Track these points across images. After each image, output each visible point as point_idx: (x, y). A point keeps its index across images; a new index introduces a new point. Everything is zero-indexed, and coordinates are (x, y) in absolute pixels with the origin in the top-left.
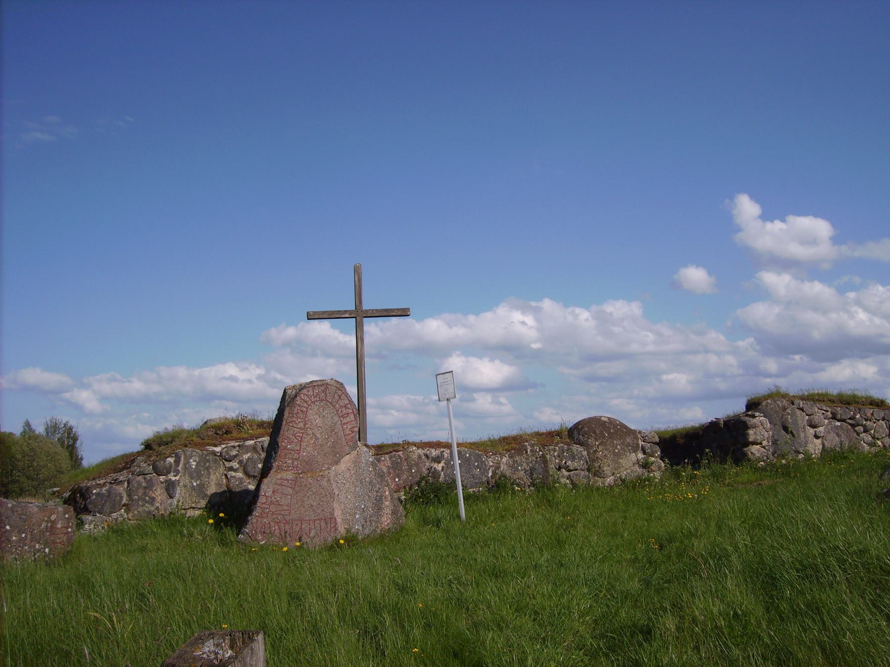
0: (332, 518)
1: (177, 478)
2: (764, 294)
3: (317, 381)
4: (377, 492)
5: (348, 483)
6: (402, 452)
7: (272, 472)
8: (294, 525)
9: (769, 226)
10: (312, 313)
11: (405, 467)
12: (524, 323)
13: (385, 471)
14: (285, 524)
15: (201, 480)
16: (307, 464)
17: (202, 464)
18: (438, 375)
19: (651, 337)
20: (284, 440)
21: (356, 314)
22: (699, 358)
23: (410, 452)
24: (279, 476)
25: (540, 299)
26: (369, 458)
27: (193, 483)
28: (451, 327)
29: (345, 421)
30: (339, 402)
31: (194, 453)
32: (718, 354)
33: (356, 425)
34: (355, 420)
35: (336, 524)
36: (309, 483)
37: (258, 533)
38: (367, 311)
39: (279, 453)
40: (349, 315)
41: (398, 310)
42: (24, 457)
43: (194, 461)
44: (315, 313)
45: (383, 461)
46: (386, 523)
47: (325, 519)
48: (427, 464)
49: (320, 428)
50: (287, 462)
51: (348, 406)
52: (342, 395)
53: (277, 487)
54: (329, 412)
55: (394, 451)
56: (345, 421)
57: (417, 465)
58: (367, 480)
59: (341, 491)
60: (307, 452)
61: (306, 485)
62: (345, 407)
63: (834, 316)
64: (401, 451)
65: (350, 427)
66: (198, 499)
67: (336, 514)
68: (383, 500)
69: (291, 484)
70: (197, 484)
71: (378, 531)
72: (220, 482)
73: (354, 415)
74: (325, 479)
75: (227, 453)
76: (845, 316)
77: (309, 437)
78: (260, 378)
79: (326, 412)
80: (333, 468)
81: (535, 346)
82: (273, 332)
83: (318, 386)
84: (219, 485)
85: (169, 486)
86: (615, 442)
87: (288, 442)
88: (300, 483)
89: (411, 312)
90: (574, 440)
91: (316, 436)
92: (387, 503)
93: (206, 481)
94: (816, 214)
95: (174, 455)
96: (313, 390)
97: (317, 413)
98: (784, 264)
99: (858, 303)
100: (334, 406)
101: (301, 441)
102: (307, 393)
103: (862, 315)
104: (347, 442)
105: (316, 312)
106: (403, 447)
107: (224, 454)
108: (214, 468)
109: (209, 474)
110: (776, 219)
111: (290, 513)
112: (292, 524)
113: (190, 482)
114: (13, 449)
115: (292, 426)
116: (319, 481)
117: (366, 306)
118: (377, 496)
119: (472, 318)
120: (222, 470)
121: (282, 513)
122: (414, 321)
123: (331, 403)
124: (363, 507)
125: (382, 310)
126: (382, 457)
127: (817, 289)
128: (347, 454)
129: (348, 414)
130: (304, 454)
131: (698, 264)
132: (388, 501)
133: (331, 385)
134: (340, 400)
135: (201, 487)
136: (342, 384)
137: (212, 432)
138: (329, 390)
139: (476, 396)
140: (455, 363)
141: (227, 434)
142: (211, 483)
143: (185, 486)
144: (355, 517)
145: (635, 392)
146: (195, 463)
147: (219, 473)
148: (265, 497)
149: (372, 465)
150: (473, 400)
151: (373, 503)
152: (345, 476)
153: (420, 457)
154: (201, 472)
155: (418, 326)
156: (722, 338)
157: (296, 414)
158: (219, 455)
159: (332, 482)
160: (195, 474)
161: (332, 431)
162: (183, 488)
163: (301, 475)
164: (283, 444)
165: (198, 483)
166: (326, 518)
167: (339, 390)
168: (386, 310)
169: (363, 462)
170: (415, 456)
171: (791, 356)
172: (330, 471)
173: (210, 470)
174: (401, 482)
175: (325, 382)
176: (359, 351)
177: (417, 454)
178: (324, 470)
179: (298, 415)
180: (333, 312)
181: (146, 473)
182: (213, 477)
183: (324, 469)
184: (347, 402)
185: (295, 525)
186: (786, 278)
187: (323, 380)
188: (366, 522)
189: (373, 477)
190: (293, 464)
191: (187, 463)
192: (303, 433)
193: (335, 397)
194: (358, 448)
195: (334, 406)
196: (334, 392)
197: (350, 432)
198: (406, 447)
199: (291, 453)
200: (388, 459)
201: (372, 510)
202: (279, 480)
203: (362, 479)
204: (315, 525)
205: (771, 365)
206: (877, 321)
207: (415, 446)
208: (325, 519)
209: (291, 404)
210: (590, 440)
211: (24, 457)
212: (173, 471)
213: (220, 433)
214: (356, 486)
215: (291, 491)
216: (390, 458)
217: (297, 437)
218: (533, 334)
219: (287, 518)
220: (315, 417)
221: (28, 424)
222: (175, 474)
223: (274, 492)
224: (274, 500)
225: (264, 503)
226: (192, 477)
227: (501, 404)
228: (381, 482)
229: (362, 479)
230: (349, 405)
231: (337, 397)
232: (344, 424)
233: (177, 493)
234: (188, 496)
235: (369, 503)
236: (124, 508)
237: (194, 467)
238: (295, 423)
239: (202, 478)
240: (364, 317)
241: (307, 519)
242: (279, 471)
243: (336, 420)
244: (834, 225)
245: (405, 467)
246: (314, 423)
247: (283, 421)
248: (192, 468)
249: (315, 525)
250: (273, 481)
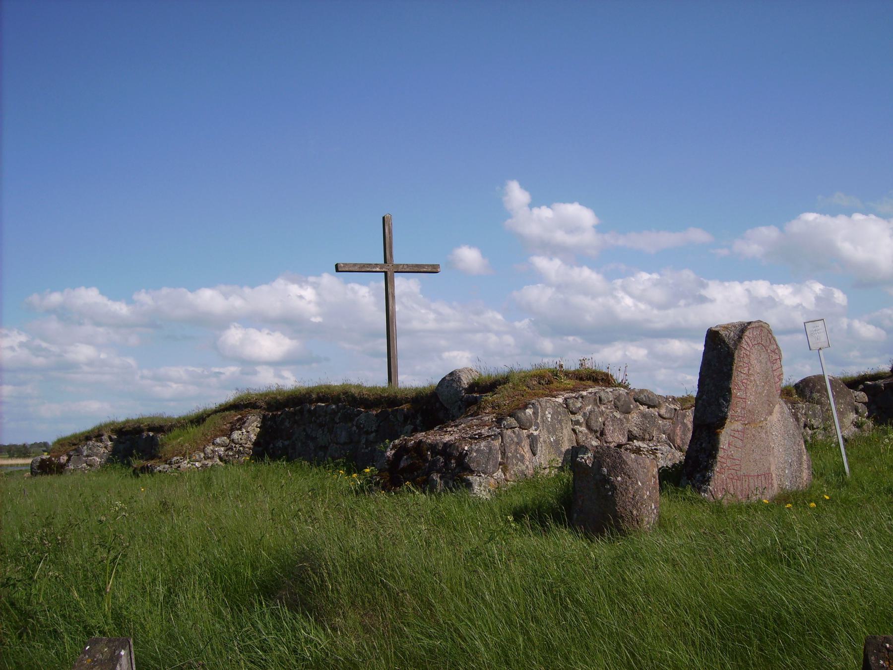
2: (537, 277)
9: (536, 211)
12: (301, 297)
15: (557, 435)
18: (806, 323)
19: (432, 316)
21: (387, 269)
22: (479, 337)
25: (319, 275)
28: (227, 299)
32: (498, 333)
38: (398, 265)
41: (428, 265)
43: (549, 413)
63: (600, 300)
67: (772, 469)
76: (612, 302)
78: (22, 345)
81: (318, 320)
82: (35, 298)
84: (570, 440)
85: (533, 441)
86: (840, 401)
90: (806, 398)
94: (584, 203)
98: (551, 249)
99: (625, 289)
103: (628, 301)
105: (346, 264)
110: (543, 205)
111: (740, 468)
119: (247, 290)
120: (570, 426)
122: (184, 290)
124: (790, 461)
125: (413, 266)
127: (587, 274)
131: (472, 245)
135: (557, 442)
139: (258, 368)
140: (234, 335)
145: (418, 368)
150: (255, 373)
155: (190, 296)
156: (499, 317)
160: (552, 430)
162: (543, 445)
168: (417, 266)
171: (565, 338)
176: (391, 307)
180: (364, 265)
181: (513, 426)
182: (565, 431)
186: (557, 263)
195: (767, 350)
205: (547, 345)
206: (642, 306)
210: (823, 399)
217: (744, 384)
218: (313, 308)
227: (283, 377)
236: (501, 467)
240: (395, 272)
244: (597, 214)
247: (733, 366)
248: (548, 421)
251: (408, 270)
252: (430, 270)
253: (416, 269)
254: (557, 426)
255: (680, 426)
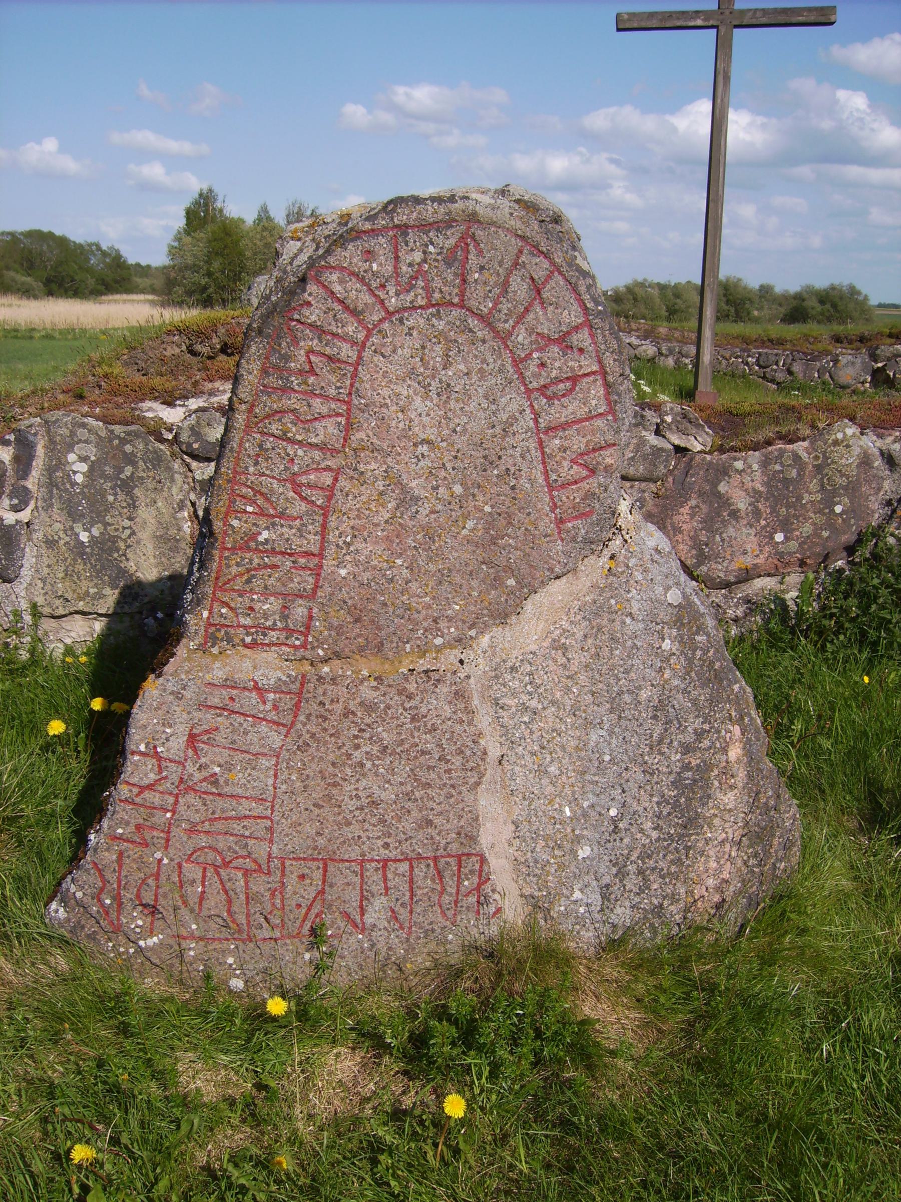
0: (469, 855)
1: (25, 516)
3: (417, 200)
4: (687, 749)
6: (806, 444)
7: (181, 651)
8: (292, 880)
10: (626, 17)
11: (811, 494)
13: (742, 506)
14: (246, 873)
16: (357, 620)
17: (108, 470)
20: (239, 504)
23: (836, 443)
24: (218, 673)
26: (668, 589)
27: (77, 535)
29: (557, 413)
30: (531, 316)
31: (82, 433)
33: (610, 437)
34: (611, 411)
35: (484, 878)
36: (362, 704)
37: (129, 906)
38: (742, 12)
39: (215, 565)
40: (704, 20)
41: (809, 10)
42: (255, 254)
43: (83, 459)
44: (632, 15)
45: (740, 472)
46: (711, 882)
47: (435, 859)
48: (887, 485)
49: (424, 449)
50: (257, 606)
51: (575, 339)
52: (549, 277)
53: (208, 718)
54: (476, 365)
55: (781, 437)
56: (557, 413)
57: (852, 489)
58: (644, 695)
60: (357, 563)
62: (563, 341)
64: (804, 440)
65: (578, 443)
66: (96, 585)
68: (709, 786)
69: (275, 707)
70: (92, 537)
71: (674, 911)
72: (173, 532)
73: (607, 385)
74: (443, 689)
75: (195, 431)
80: (485, 640)
83: (424, 227)
89: (840, 16)
91: (404, 489)
92: (729, 799)
93: (124, 528)
95: (12, 437)
96: (396, 251)
97: (412, 373)
100: (504, 338)
101: (326, 512)
102: (359, 265)
104: (560, 521)
106: (813, 427)
107: (184, 437)
108: (151, 484)
109: (133, 506)
111: (270, 830)
112: (283, 874)
113: (70, 531)
114: (243, 243)
115: (284, 437)
116: (410, 697)
118: (687, 767)
121: (236, 827)
123: (486, 320)
125: (776, 11)
126: (735, 459)
128: (558, 577)
129: (574, 379)
130: (343, 572)
132: (732, 787)
133: (493, 223)
136: (557, 219)
137: (179, 346)
138: (480, 253)
141: (229, 355)
142: (139, 534)
143: (51, 543)
144: (574, 853)
146: (83, 467)
147: (168, 501)
148: (151, 762)
149: (678, 622)
151: (664, 800)
153: (865, 461)
154: (104, 496)
157: (301, 372)
158: (170, 437)
159: (476, 702)
161: (490, 462)
163: (326, 669)
164: (235, 523)
165: (96, 532)
166: (441, 852)
167: (537, 250)
168: (785, 11)
169: (635, 607)
170: (849, 460)
172: (466, 655)
173: (136, 491)
174: (793, 545)
175: (459, 205)
177: (856, 451)
178: (439, 649)
179: (311, 380)
180: (670, 15)
182: (145, 513)
183: (439, 641)
185: (294, 877)
187: (452, 199)
188: (622, 874)
189: (676, 682)
190: (284, 617)
191: (56, 465)
192: (337, 473)
193: (513, 286)
194: (618, 541)
195: (504, 338)
196: (508, 264)
197: (577, 471)
198: (820, 425)
199: (274, 567)
200: (755, 467)
201: (657, 828)
202: (216, 691)
203: (620, 693)
204: (385, 880)
207: (852, 419)
208: (435, 859)
209: (277, 320)
211: (255, 254)
212: (7, 491)
213: (204, 349)
214: (588, 725)
215: (276, 739)
216: (765, 463)
219: (261, 850)
220: (398, 389)
221: (264, 210)
222: (16, 501)
223: (192, 739)
224: (198, 776)
225: (150, 787)
226: (73, 515)
228: (713, 701)
229: (620, 693)
230: (584, 334)
231: (520, 288)
232: (549, 429)
233: (27, 565)
234: (61, 575)
237: (79, 478)
239: (108, 519)
240: (736, 26)
241: (353, 856)
242: (215, 651)
243: (514, 407)
245: (811, 494)
246: (397, 424)
248: (74, 484)
249: (385, 880)
251: (764, 20)
252: (812, 19)
253: (781, 19)
254: (111, 498)
255: (693, 502)
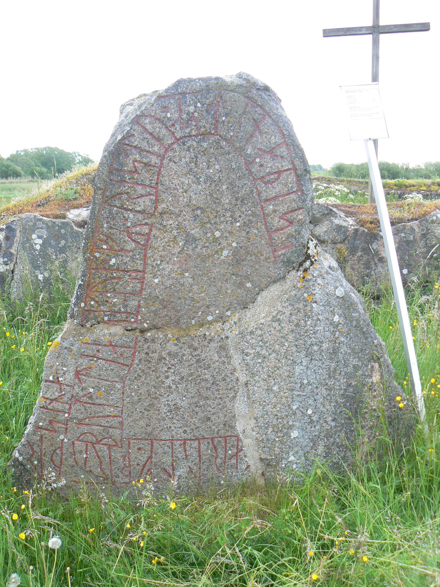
5: (274, 355)
14: (109, 447)
27: (37, 276)
43: (39, 237)
47: (212, 439)
53: (84, 362)
59: (253, 375)
61: (161, 358)
67: (239, 428)
74: (213, 345)
77: (168, 236)
79: (217, 167)
87: (111, 248)
88: (147, 353)
101: (146, 247)
115: (122, 207)
116: (195, 349)
117: (382, 22)
118: (349, 385)
130: (156, 281)
134: (257, 134)
146: (40, 241)
152: (266, 336)
157: (130, 172)
178: (210, 323)
179: (136, 176)
184: (276, 139)
192: (151, 227)
204: (185, 450)
208: (212, 439)
220: (183, 180)
223: (77, 374)
224: (81, 394)
225: (56, 400)
235: (327, 403)
238: (130, 198)
248: (35, 250)
249: (185, 450)
250: (74, 348)
